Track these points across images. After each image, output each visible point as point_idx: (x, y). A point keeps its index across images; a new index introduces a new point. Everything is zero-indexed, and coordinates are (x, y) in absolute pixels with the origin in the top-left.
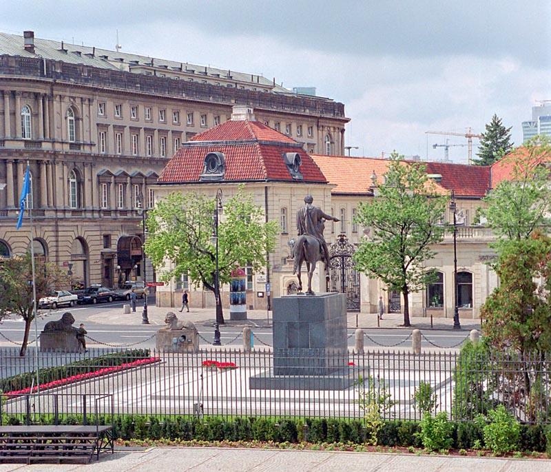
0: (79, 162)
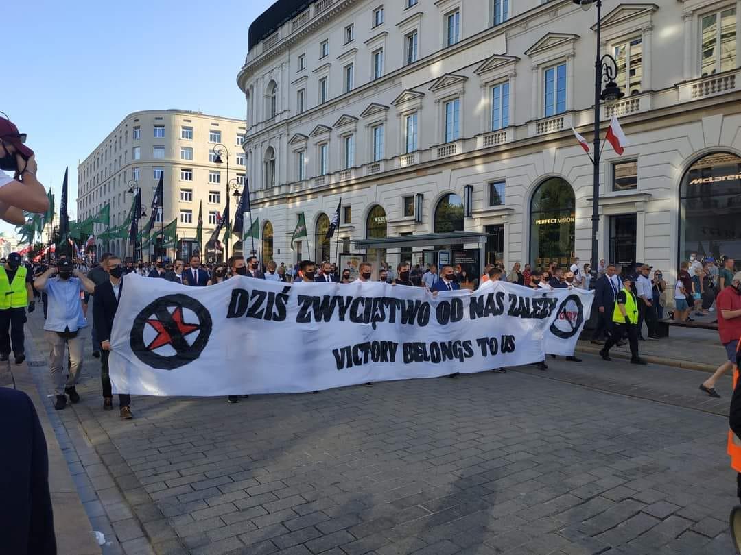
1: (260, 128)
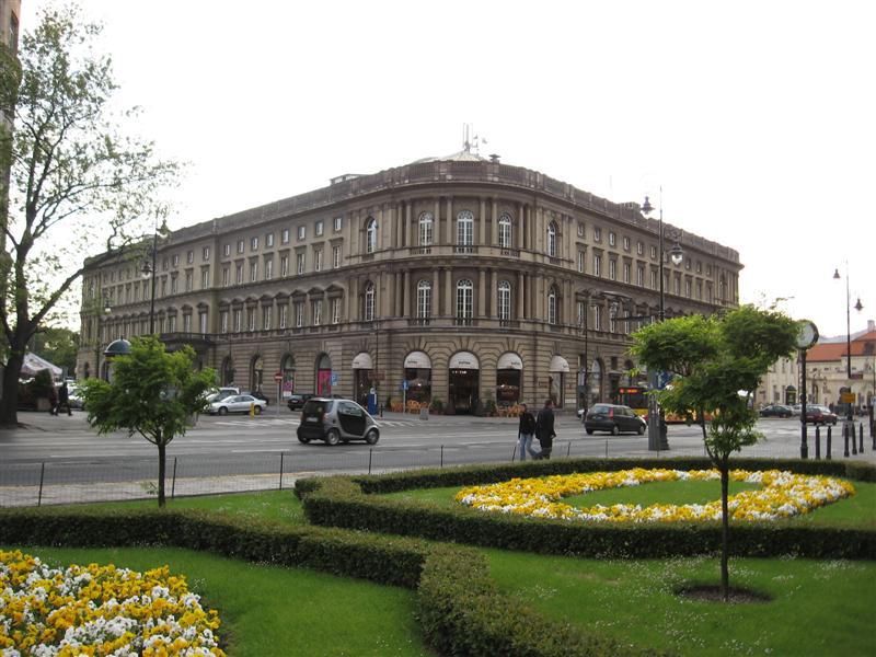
0: (558, 276)
1: (354, 262)
